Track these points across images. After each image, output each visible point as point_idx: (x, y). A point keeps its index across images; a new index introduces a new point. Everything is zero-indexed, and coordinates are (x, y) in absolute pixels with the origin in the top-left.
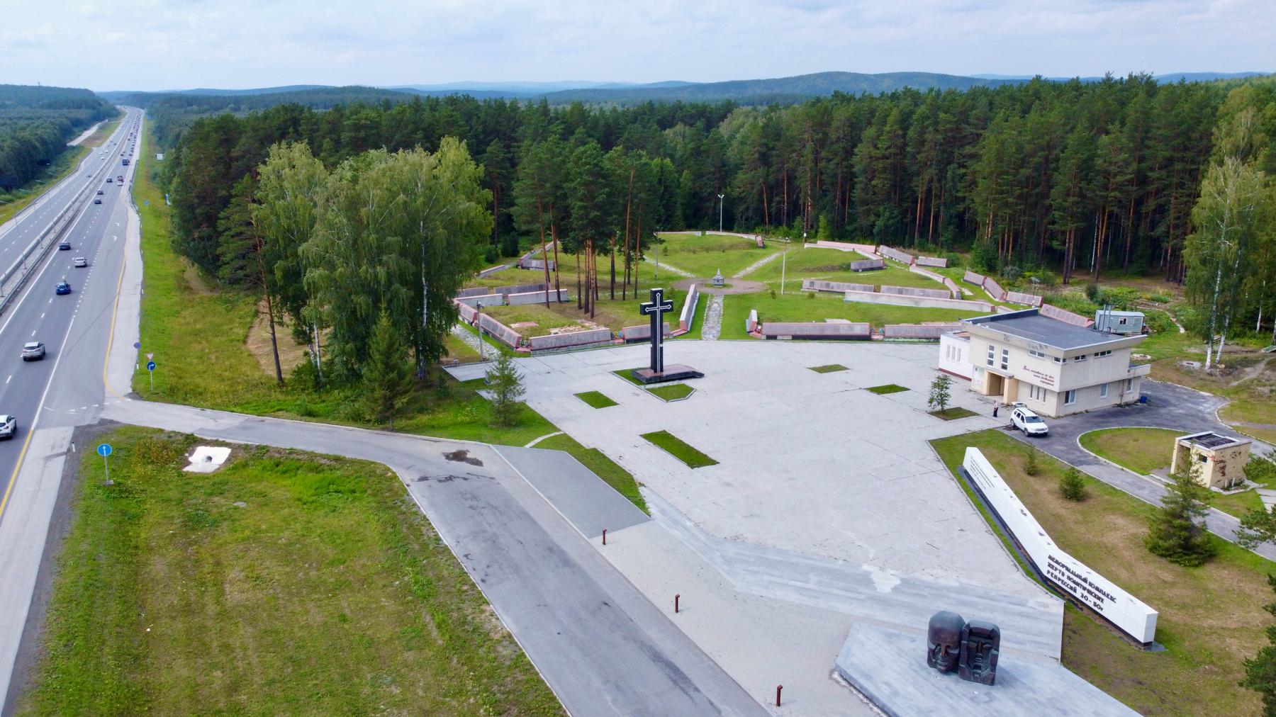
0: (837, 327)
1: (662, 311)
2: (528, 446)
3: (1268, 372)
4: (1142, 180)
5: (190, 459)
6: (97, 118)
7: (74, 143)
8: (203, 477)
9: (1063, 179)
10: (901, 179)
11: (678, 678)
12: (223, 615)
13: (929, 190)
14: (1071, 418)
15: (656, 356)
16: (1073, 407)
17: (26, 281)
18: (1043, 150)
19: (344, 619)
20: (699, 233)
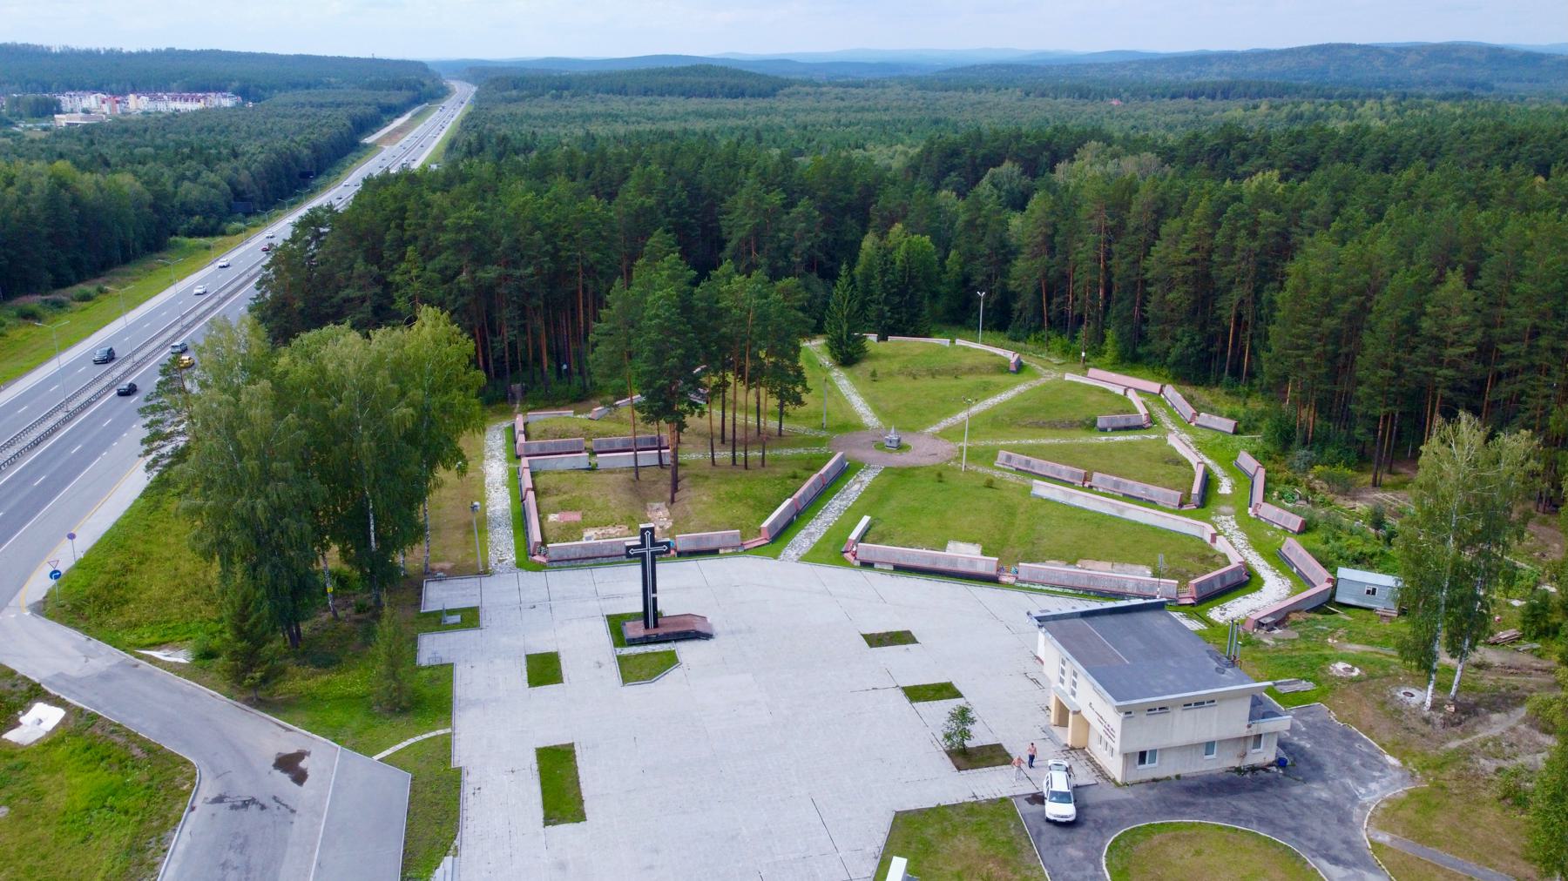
0: (953, 560)
1: (653, 554)
2: (376, 758)
3: (1523, 727)
4: (1485, 351)
5: (22, 719)
6: (417, 101)
7: (368, 140)
9: (1374, 345)
10: (1205, 293)
13: (1239, 317)
14: (1142, 789)
15: (649, 585)
16: (1149, 771)
18: (1360, 293)
20: (946, 342)
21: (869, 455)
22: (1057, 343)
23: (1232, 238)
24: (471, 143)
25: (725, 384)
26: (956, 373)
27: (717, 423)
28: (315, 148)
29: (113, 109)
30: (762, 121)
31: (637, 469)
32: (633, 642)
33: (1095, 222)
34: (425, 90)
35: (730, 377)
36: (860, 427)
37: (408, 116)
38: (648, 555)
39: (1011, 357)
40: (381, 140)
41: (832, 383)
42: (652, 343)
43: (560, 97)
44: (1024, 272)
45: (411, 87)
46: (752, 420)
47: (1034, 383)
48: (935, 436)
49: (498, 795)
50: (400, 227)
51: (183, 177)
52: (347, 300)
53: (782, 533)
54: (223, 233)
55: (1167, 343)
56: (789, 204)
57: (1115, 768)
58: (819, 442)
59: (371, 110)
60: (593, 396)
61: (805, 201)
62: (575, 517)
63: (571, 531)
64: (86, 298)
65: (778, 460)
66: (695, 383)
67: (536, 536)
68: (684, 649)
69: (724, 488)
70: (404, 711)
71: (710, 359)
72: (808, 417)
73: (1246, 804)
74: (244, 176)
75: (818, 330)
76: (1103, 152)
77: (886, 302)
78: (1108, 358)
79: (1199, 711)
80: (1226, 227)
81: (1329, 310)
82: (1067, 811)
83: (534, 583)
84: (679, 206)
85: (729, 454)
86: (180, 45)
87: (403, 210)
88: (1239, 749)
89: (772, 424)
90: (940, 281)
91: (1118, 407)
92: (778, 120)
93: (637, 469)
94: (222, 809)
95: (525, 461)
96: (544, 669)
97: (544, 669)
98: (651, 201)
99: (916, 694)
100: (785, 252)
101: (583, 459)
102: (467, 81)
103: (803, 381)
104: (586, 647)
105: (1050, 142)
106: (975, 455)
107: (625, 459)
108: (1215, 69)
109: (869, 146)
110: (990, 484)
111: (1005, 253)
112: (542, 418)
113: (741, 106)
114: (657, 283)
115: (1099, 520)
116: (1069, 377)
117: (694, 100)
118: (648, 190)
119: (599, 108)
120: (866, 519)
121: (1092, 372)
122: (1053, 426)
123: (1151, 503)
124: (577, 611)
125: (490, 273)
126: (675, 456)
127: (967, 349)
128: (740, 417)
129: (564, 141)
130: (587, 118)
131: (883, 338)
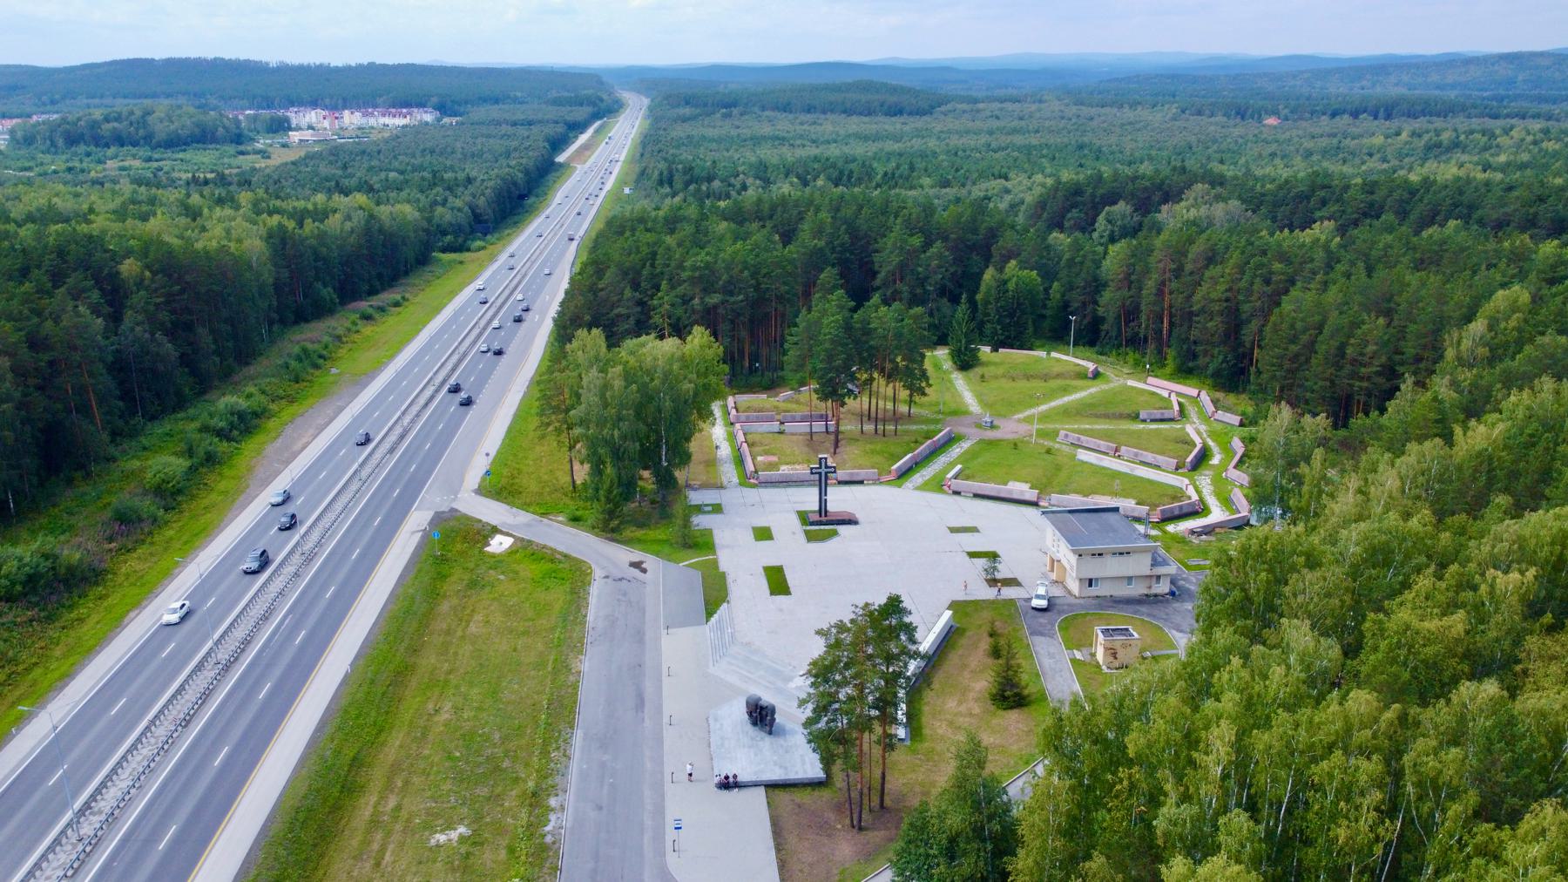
0: (1010, 491)
6: (596, 116)
7: (560, 159)
8: (493, 556)
11: (640, 704)
12: (463, 637)
15: (823, 502)
16: (1094, 591)
17: (402, 437)
19: (515, 650)
20: (1042, 354)
21: (972, 431)
22: (1131, 356)
23: (1252, 284)
24: (661, 168)
25: (871, 380)
26: (1046, 378)
27: (866, 406)
28: (527, 172)
29: (332, 124)
30: (917, 143)
31: (811, 433)
32: (812, 524)
33: (1161, 265)
34: (603, 106)
35: (876, 375)
36: (966, 413)
37: (590, 131)
38: (822, 478)
39: (1091, 366)
40: (571, 158)
41: (950, 381)
42: (826, 350)
43: (728, 116)
44: (1109, 301)
45: (592, 103)
46: (890, 406)
47: (1105, 387)
48: (1019, 421)
49: (745, 581)
50: (653, 265)
51: (435, 203)
52: (619, 315)
53: (904, 474)
54: (468, 250)
55: (1207, 359)
56: (927, 244)
57: (1074, 587)
58: (936, 421)
59: (560, 129)
60: (779, 386)
61: (938, 244)
62: (775, 459)
63: (772, 466)
64: (397, 304)
65: (907, 432)
66: (852, 378)
67: (750, 467)
68: (841, 529)
69: (869, 447)
70: (690, 547)
71: (862, 361)
72: (931, 405)
73: (1144, 609)
74: (482, 201)
75: (942, 341)
76: (1208, 193)
77: (999, 322)
78: (1168, 370)
79: (1121, 558)
80: (1246, 277)
81: (1294, 340)
82: (1043, 603)
83: (752, 494)
84: (842, 245)
85: (872, 427)
86: (380, 60)
87: (654, 254)
88: (1147, 583)
89: (903, 408)
90: (1044, 306)
91: (1161, 404)
92: (932, 143)
93: (811, 433)
94: (609, 581)
95: (738, 426)
96: (763, 534)
97: (763, 534)
98: (821, 244)
99: (972, 555)
100: (922, 282)
101: (775, 426)
102: (639, 92)
103: (927, 379)
104: (787, 527)
105: (1163, 183)
106: (1043, 434)
107: (803, 427)
108: (1393, 79)
109: (1012, 175)
110: (1049, 452)
111: (1097, 285)
112: (746, 399)
113: (898, 126)
114: (827, 311)
115: (1116, 475)
116: (1131, 383)
117: (855, 118)
118: (818, 232)
119: (767, 130)
120: (959, 467)
121: (1151, 380)
122: (1107, 416)
123: (1158, 467)
124: (784, 508)
125: (714, 299)
126: (838, 424)
127: (1058, 360)
128: (881, 403)
129: (741, 169)
130: (757, 141)
131: (995, 350)
